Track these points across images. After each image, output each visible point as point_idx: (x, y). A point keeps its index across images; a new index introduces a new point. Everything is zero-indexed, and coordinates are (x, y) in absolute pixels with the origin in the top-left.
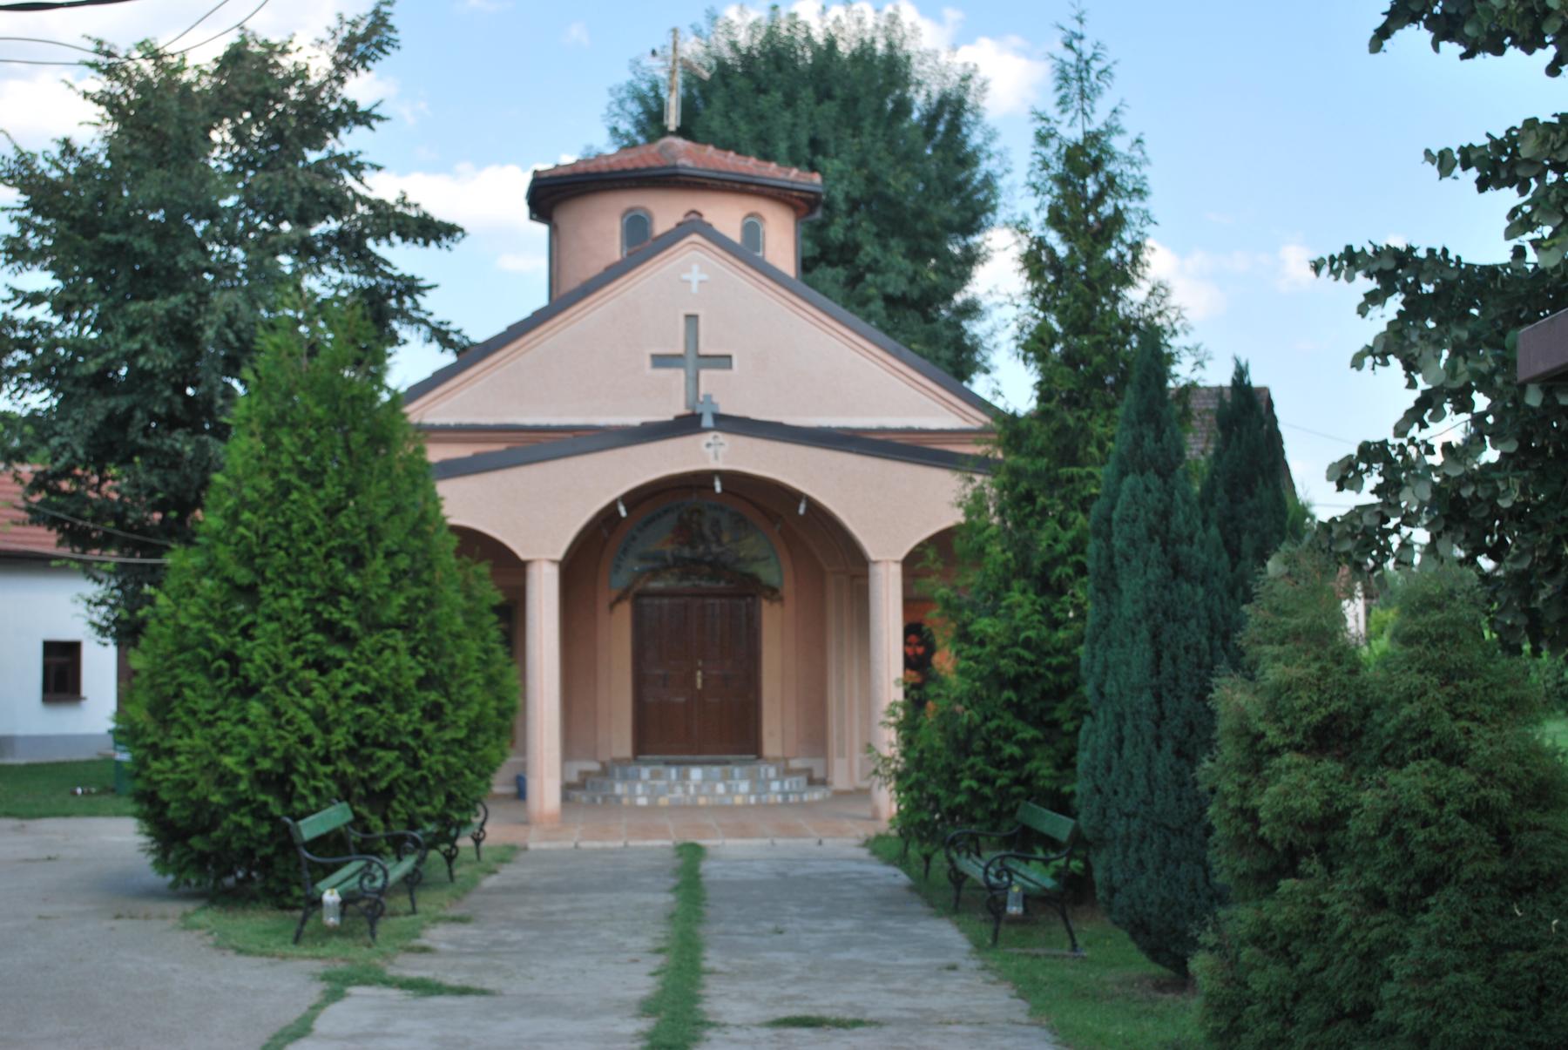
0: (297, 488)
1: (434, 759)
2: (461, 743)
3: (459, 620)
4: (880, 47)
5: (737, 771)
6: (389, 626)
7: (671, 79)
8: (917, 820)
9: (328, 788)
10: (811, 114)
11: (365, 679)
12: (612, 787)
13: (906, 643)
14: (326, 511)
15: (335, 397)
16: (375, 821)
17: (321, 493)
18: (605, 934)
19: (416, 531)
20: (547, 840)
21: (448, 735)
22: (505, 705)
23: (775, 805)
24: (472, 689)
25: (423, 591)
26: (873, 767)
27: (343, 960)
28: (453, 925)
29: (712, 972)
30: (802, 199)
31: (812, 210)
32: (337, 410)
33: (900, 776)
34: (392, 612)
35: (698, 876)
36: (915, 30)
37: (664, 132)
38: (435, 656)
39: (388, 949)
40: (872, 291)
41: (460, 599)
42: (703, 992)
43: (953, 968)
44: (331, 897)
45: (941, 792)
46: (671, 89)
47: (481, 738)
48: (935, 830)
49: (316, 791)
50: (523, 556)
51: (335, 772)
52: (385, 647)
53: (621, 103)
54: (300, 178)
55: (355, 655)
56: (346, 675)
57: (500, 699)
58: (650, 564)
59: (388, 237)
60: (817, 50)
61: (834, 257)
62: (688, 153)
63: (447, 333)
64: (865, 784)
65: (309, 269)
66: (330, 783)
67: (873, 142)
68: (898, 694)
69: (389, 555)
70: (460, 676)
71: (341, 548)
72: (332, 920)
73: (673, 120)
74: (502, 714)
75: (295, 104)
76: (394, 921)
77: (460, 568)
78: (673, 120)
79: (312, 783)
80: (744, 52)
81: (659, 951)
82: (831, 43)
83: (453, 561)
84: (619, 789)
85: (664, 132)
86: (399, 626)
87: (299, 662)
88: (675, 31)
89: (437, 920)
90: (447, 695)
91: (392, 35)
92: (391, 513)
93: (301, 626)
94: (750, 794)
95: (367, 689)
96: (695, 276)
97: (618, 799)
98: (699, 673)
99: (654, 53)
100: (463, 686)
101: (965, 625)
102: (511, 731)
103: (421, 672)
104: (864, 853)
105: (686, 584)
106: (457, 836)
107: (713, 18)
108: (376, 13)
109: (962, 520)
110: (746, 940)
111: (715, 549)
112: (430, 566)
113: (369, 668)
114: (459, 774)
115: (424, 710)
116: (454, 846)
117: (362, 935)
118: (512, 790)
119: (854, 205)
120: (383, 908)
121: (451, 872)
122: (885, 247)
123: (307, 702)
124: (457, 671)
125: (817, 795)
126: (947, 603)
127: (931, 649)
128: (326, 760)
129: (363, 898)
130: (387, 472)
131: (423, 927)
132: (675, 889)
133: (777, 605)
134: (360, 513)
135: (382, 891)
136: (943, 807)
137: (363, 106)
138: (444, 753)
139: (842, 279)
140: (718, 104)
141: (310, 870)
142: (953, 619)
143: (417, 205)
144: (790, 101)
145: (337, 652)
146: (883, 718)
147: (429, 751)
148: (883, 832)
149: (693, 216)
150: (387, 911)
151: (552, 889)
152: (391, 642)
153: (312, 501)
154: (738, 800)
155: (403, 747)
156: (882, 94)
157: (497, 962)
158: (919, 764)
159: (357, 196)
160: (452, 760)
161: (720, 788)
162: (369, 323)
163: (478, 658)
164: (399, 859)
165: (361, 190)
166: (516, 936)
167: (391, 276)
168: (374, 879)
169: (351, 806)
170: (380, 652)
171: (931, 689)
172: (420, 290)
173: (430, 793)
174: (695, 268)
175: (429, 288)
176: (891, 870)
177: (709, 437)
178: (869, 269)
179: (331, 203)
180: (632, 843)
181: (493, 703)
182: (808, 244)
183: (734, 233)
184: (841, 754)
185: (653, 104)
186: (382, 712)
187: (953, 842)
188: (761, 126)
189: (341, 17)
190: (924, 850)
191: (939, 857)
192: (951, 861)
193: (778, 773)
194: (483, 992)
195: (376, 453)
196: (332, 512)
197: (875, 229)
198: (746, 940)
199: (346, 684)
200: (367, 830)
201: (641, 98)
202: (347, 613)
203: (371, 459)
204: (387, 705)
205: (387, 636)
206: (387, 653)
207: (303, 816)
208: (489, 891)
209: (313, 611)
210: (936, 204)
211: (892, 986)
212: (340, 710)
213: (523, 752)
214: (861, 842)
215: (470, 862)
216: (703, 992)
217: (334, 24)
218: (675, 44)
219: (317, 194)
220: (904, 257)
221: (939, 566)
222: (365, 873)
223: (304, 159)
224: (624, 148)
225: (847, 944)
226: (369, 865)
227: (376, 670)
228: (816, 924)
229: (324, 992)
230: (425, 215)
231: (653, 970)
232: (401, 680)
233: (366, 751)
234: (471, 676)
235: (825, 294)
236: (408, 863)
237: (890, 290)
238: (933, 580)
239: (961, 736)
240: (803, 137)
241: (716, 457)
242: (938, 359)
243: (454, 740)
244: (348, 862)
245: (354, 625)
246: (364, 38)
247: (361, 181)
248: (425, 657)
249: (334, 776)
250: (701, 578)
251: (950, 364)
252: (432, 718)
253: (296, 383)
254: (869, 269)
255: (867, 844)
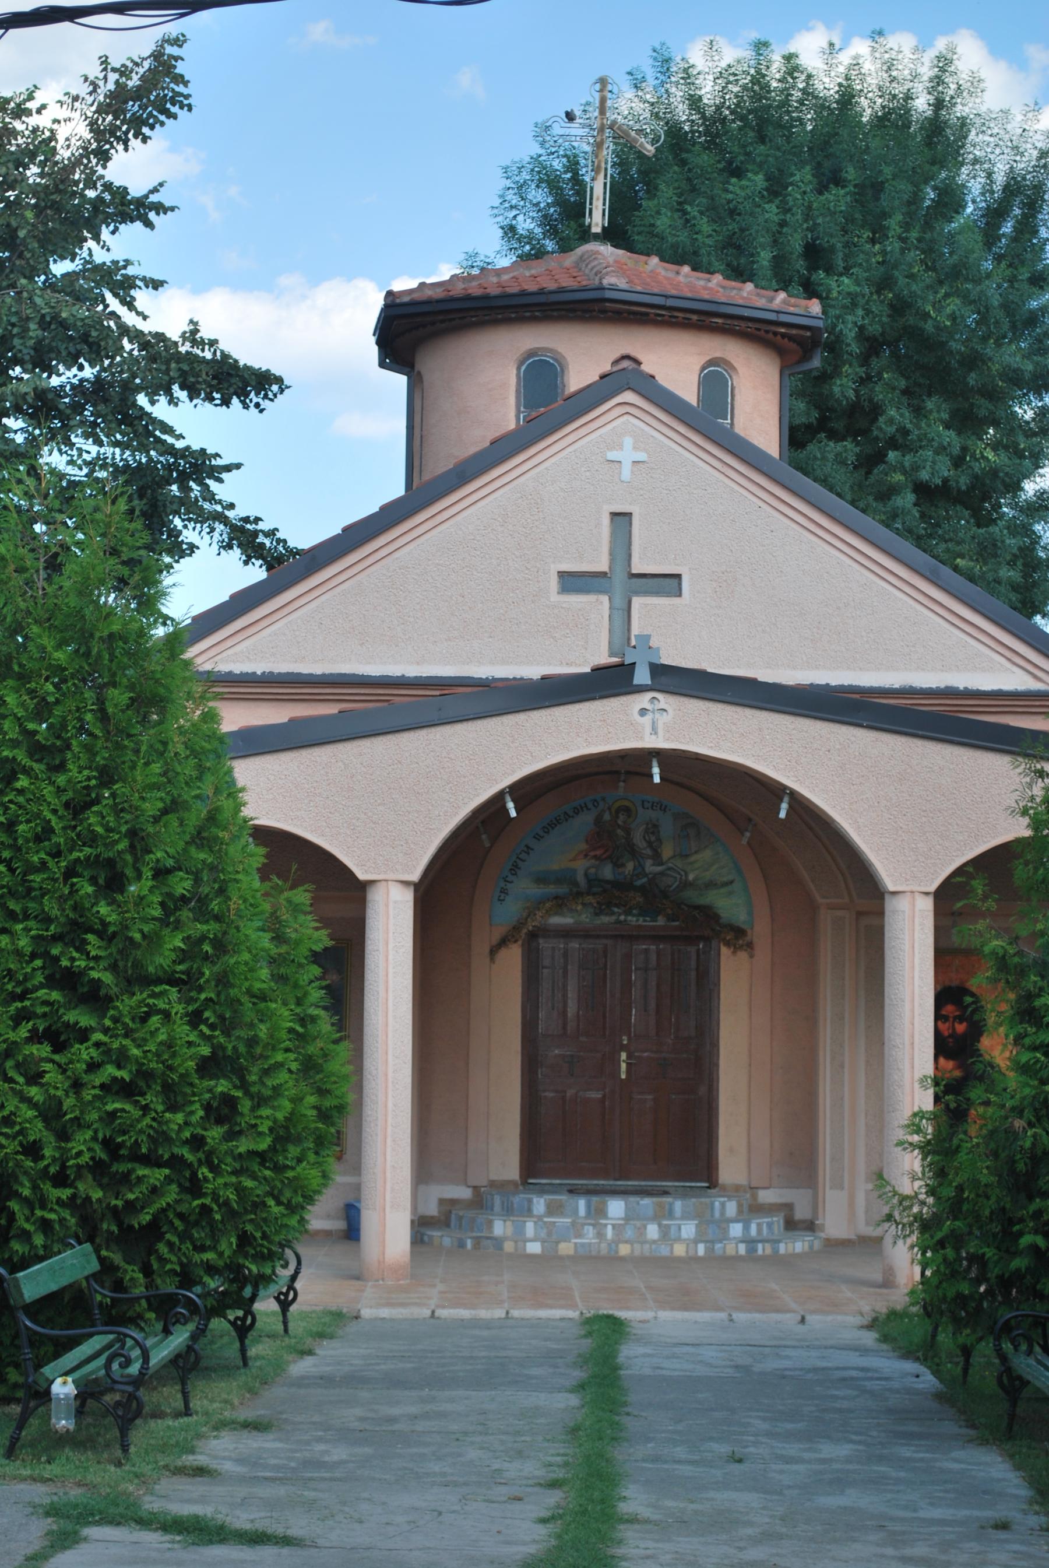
0: (27, 771)
1: (220, 1181)
2: (262, 1157)
3: (264, 973)
4: (922, 104)
5: (678, 1205)
6: (159, 981)
7: (596, 154)
8: (951, 1294)
9: (62, 1221)
10: (810, 207)
11: (121, 1059)
12: (490, 1224)
13: (938, 1016)
14: (67, 805)
15: (86, 636)
16: (133, 1273)
17: (61, 780)
18: (473, 1454)
19: (200, 838)
20: (389, 1305)
21: (243, 1146)
22: (328, 1102)
23: (737, 1258)
24: (282, 1076)
25: (211, 928)
26: (886, 1210)
27: (79, 1484)
28: (245, 1433)
29: (633, 1520)
30: (791, 338)
31: (806, 355)
32: (87, 654)
33: (926, 1226)
34: (162, 960)
35: (616, 1368)
36: (976, 82)
37: (585, 235)
38: (227, 1026)
39: (147, 1469)
40: (898, 477)
41: (265, 941)
42: (619, 1551)
43: (1003, 1526)
44: (63, 1388)
45: (989, 1252)
46: (596, 170)
47: (293, 1151)
48: (979, 1309)
49: (45, 1226)
50: (362, 876)
51: (74, 1197)
52: (152, 1011)
53: (521, 188)
54: (38, 300)
55: (108, 1022)
56: (94, 1052)
57: (322, 1092)
58: (552, 889)
59: (169, 392)
60: (821, 106)
61: (839, 425)
62: (620, 268)
63: (255, 533)
64: (878, 1232)
65: (52, 436)
66: (66, 1214)
67: (902, 251)
68: (925, 1100)
69: (161, 873)
70: (263, 1057)
71: (88, 862)
72: (63, 1423)
73: (597, 219)
74: (324, 1115)
75: (35, 190)
76: (157, 1425)
77: (266, 894)
78: (597, 219)
79: (39, 1213)
80: (710, 111)
81: (554, 1484)
82: (847, 97)
83: (257, 884)
84: (499, 1228)
85: (585, 235)
86: (172, 981)
87: (23, 1032)
88: (603, 82)
89: (221, 1425)
90: (244, 1086)
91: (181, 89)
92: (165, 812)
93: (26, 978)
94: (696, 1242)
95: (124, 1074)
96: (627, 454)
97: (498, 1243)
98: (624, 1056)
99: (570, 117)
100: (266, 1072)
101: (1030, 997)
102: (339, 1138)
103: (206, 1051)
104: (869, 1338)
105: (605, 919)
106: (253, 1299)
107: (664, 63)
108: (157, 55)
109: (1028, 833)
110: (687, 1470)
111: (650, 867)
112: (222, 891)
113: (127, 1042)
114: (259, 1205)
115: (208, 1108)
116: (249, 1312)
117: (107, 1446)
118: (340, 1225)
119: (872, 346)
120: (140, 1406)
121: (243, 1351)
122: (918, 411)
123: (34, 1091)
124: (258, 1050)
125: (799, 1245)
126: (1002, 962)
127: (977, 1030)
128: (61, 1180)
129: (111, 1390)
130: (162, 746)
131: (199, 1436)
132: (581, 1387)
133: (743, 955)
134: (118, 810)
135: (138, 1381)
136: (994, 1272)
137: (136, 191)
138: (235, 1173)
139: (851, 458)
140: (667, 192)
141: (32, 1344)
142: (1011, 986)
143: (213, 343)
144: (776, 188)
145: (81, 1017)
146: (901, 1134)
147: (214, 1169)
148: (899, 1307)
149: (626, 364)
150: (146, 1410)
151: (394, 1382)
152: (161, 1004)
153: (48, 791)
154: (679, 1250)
155: (176, 1162)
156: (920, 178)
157: (309, 1494)
158: (955, 1207)
159: (125, 330)
160: (249, 1183)
161: (653, 1231)
162: (138, 525)
163: (291, 1030)
164: (167, 1332)
165: (129, 318)
166: (339, 1453)
167: (171, 450)
168: (128, 1362)
169: (97, 1251)
170: (144, 1019)
171: (976, 1093)
172: (216, 473)
173: (215, 1233)
174: (628, 442)
175: (228, 468)
176: (911, 1366)
177: (643, 700)
178: (893, 443)
179: (85, 338)
180: (516, 1313)
181: (311, 1099)
182: (802, 406)
183: (688, 392)
184: (838, 1185)
185: (569, 192)
186: (145, 1109)
187: (1007, 1328)
188: (733, 226)
189: (104, 61)
190: (961, 1340)
191: (985, 1349)
192: (1003, 1358)
193: (740, 1211)
194: (286, 1541)
195: (144, 720)
196: (78, 807)
197: (903, 383)
198: (687, 1470)
199: (93, 1067)
200: (119, 1286)
201: (549, 181)
202: (97, 958)
203: (138, 729)
204: (153, 1099)
205: (154, 995)
206: (155, 1020)
207: (24, 1264)
208: (301, 1382)
209: (46, 955)
210: (998, 344)
211: (908, 1552)
212: (84, 1106)
213: (357, 1169)
214: (865, 1321)
215: (272, 1336)
216: (619, 1551)
217: (95, 71)
218: (603, 101)
219: (64, 325)
220: (947, 427)
221: (991, 904)
222: (115, 1353)
223: (47, 271)
224: (524, 258)
225: (840, 1483)
226: (122, 1339)
227: (139, 1046)
228: (792, 1449)
229: (49, 1533)
230: (225, 356)
231: (545, 1514)
232: (177, 1061)
233: (122, 1167)
234: (280, 1057)
235: (824, 482)
236: (180, 1338)
237: (924, 475)
238: (981, 925)
239: (1021, 1166)
240: (796, 243)
241: (654, 731)
242: (998, 581)
243: (252, 1153)
244: (91, 1335)
245: (107, 978)
246: (138, 94)
247: (130, 305)
248: (212, 1027)
249: (71, 1203)
250: (628, 912)
251: (1015, 588)
252: (219, 1121)
253: (29, 613)
254: (893, 443)
255: (872, 1325)
